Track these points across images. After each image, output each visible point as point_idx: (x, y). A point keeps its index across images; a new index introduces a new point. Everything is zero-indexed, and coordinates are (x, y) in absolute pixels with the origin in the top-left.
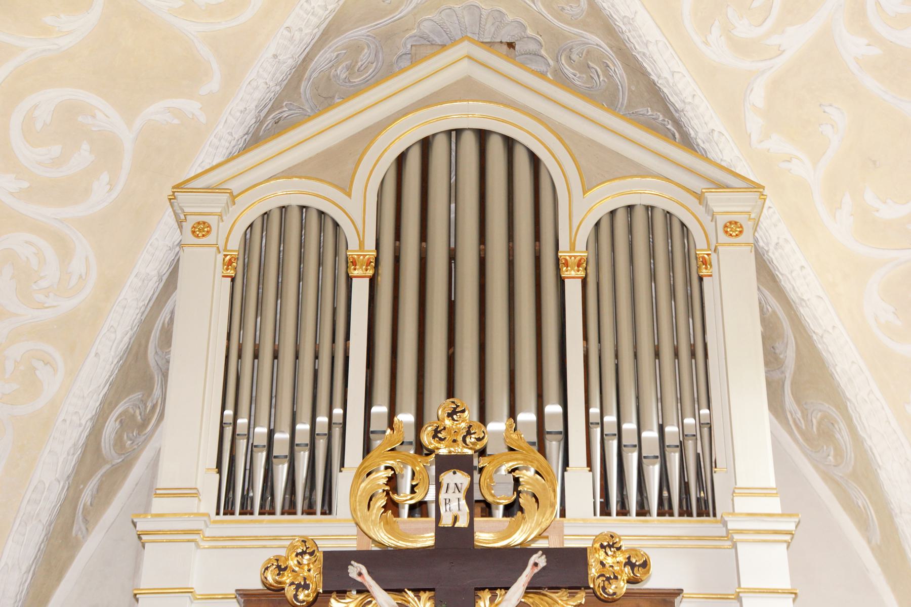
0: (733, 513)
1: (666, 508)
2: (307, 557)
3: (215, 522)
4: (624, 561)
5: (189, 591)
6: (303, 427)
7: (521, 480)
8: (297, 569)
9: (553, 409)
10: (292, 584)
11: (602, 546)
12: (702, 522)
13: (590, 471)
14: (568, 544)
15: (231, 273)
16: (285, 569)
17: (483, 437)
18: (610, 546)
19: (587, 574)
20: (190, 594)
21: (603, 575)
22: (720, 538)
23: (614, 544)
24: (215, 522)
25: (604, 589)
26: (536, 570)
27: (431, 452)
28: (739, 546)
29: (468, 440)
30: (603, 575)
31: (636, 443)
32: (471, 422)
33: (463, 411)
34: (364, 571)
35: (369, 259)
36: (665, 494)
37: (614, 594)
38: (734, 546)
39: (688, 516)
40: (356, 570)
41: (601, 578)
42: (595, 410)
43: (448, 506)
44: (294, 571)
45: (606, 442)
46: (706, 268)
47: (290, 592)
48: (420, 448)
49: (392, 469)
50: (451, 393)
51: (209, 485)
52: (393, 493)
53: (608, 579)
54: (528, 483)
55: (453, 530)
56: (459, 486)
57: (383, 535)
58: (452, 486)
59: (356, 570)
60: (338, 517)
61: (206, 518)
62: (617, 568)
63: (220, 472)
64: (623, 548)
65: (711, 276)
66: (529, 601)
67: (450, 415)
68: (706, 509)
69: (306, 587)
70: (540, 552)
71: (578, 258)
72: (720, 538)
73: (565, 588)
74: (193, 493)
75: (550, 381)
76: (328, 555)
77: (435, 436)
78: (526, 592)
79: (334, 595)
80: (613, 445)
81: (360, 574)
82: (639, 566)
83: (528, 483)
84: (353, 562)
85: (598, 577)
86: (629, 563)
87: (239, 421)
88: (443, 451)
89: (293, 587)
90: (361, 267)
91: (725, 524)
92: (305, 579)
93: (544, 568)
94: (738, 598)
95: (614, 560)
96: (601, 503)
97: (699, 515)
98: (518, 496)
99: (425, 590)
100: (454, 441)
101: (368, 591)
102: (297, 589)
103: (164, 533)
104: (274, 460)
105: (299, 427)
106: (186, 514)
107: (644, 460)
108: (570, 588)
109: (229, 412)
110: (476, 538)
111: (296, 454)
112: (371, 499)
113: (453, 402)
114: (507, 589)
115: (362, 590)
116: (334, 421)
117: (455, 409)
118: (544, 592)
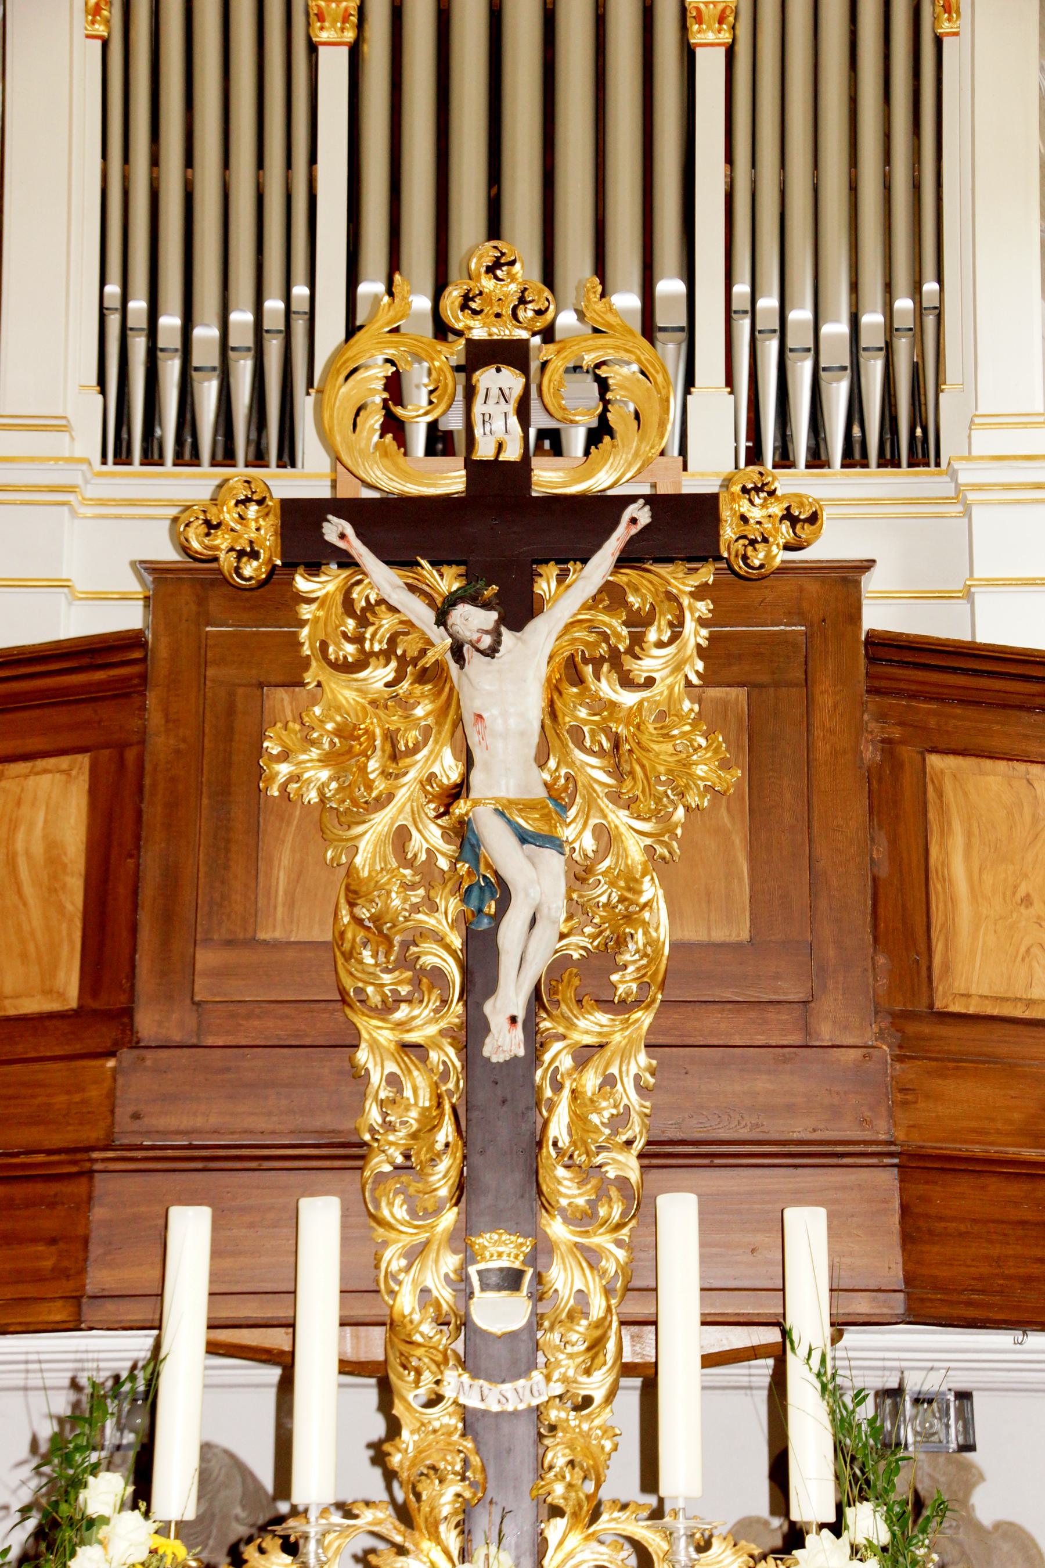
0: (969, 458)
1: (857, 455)
2: (253, 508)
3: (100, 475)
4: (780, 514)
5: (64, 585)
6: (242, 317)
7: (610, 381)
8: (238, 527)
9: (669, 286)
10: (232, 549)
11: (745, 490)
12: (917, 474)
13: (731, 393)
14: (685, 490)
15: (100, 29)
16: (218, 526)
17: (547, 309)
18: (757, 490)
19: (718, 535)
20: (66, 590)
21: (744, 537)
22: (945, 500)
23: (763, 485)
24: (100, 475)
25: (745, 558)
26: (634, 530)
27: (459, 334)
28: (976, 511)
29: (521, 314)
30: (744, 537)
31: (811, 344)
32: (525, 282)
33: (512, 263)
34: (349, 530)
35: (346, 9)
36: (856, 431)
37: (762, 566)
38: (967, 513)
39: (893, 467)
40: (336, 530)
41: (741, 542)
42: (742, 289)
43: (487, 426)
44: (232, 530)
45: (759, 344)
46: (949, 20)
47: (227, 561)
48: (442, 330)
49: (392, 362)
50: (494, 230)
51: (87, 414)
52: (396, 404)
53: (753, 542)
54: (622, 387)
55: (495, 465)
56: (507, 392)
57: (379, 473)
58: (494, 392)
59: (336, 530)
60: (307, 470)
61: (85, 467)
62: (768, 526)
63: (103, 392)
64: (778, 493)
65: (956, 34)
66: (621, 579)
67: (490, 270)
68: (923, 453)
69: (254, 555)
70: (641, 501)
71: (720, 7)
72: (945, 500)
73: (682, 560)
74: (60, 425)
75: (664, 238)
76: (287, 505)
77: (464, 307)
78: (615, 566)
79: (301, 570)
80: (771, 348)
81: (342, 536)
82: (805, 521)
83: (622, 387)
84: (330, 517)
85: (736, 541)
86: (788, 516)
87: (132, 305)
88: (479, 332)
89: (234, 554)
90: (333, 25)
91: (953, 475)
92: (251, 542)
93: (647, 527)
94: (968, 595)
95: (764, 512)
96: (747, 448)
97: (911, 465)
98: (606, 410)
99: (450, 563)
100: (498, 315)
101: (357, 565)
102: (239, 558)
103: (17, 489)
104: (195, 374)
105: (235, 317)
106: (50, 459)
107: (823, 374)
108: (690, 560)
109: (113, 289)
110: (534, 479)
111: (232, 365)
112: (357, 414)
113: (495, 247)
114: (585, 561)
115: (346, 561)
116: (294, 307)
117: (498, 258)
118: (646, 566)
